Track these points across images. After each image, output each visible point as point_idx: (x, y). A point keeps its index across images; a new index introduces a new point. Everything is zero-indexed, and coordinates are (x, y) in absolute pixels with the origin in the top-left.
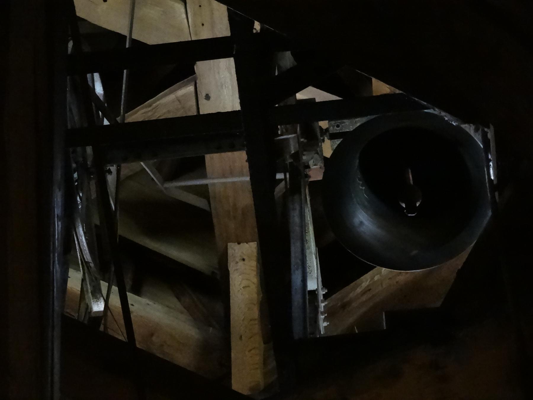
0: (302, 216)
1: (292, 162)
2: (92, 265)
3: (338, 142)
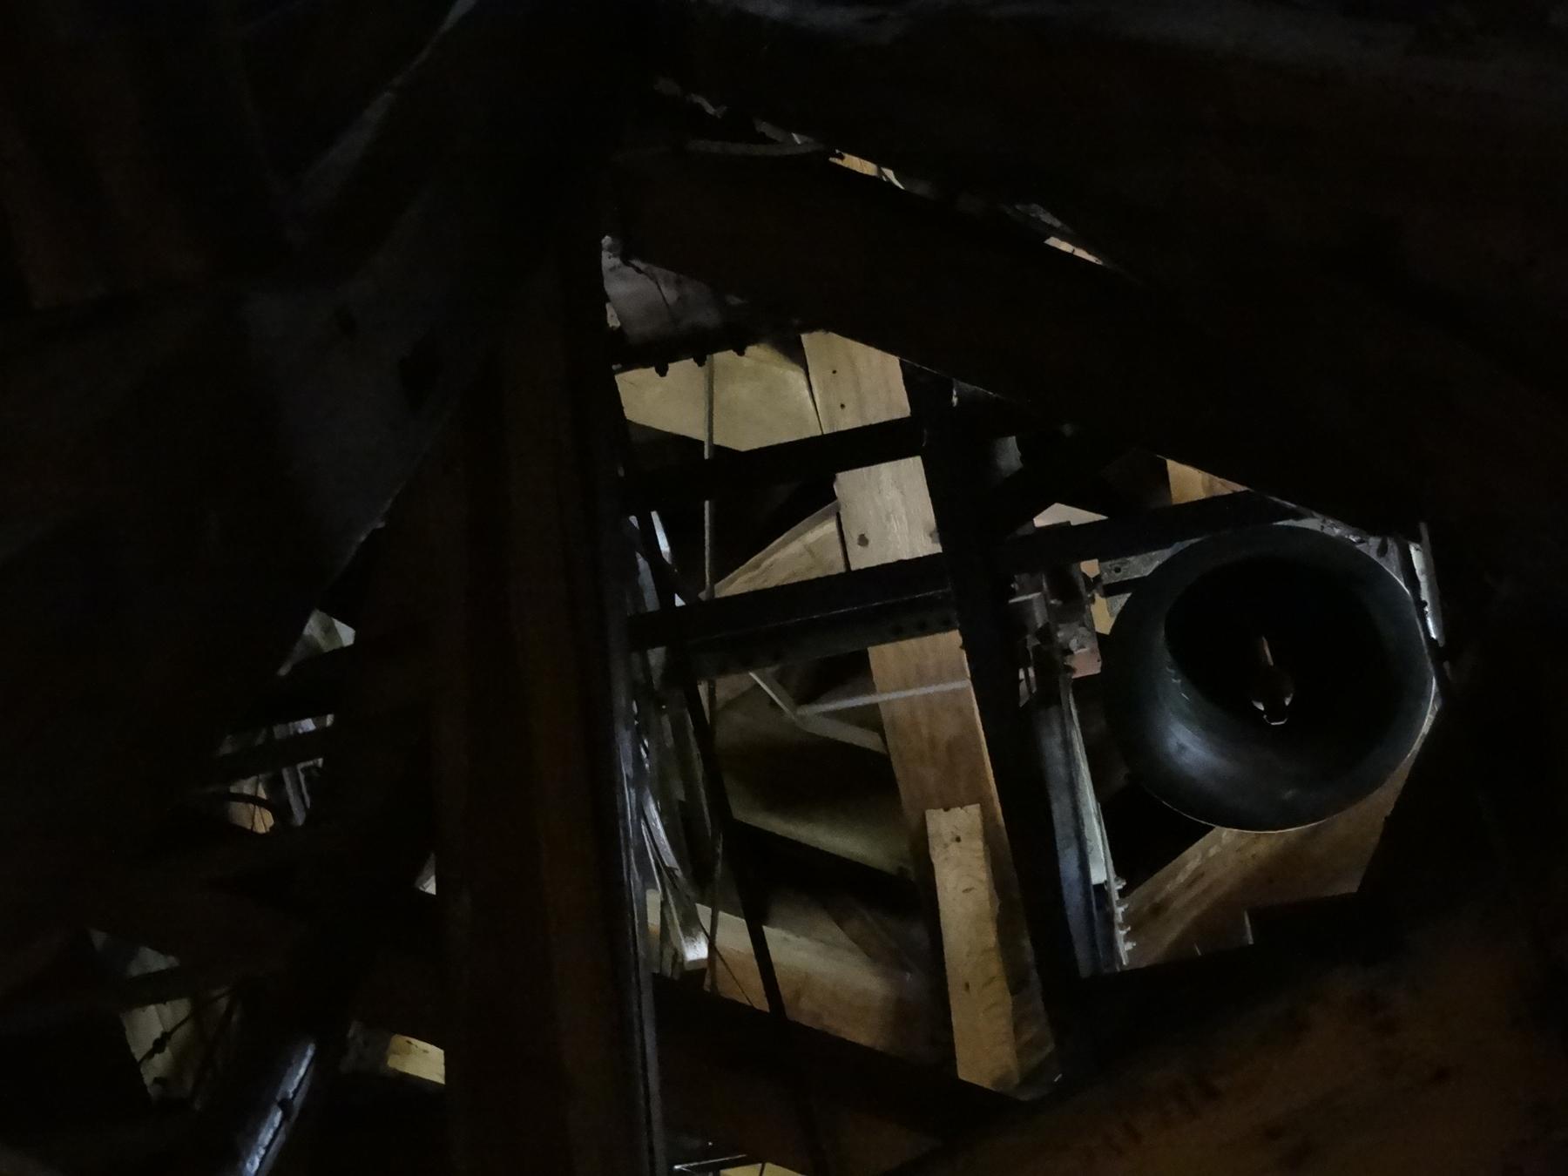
0: (1067, 745)
1: (1038, 645)
2: (679, 873)
3: (1122, 600)
